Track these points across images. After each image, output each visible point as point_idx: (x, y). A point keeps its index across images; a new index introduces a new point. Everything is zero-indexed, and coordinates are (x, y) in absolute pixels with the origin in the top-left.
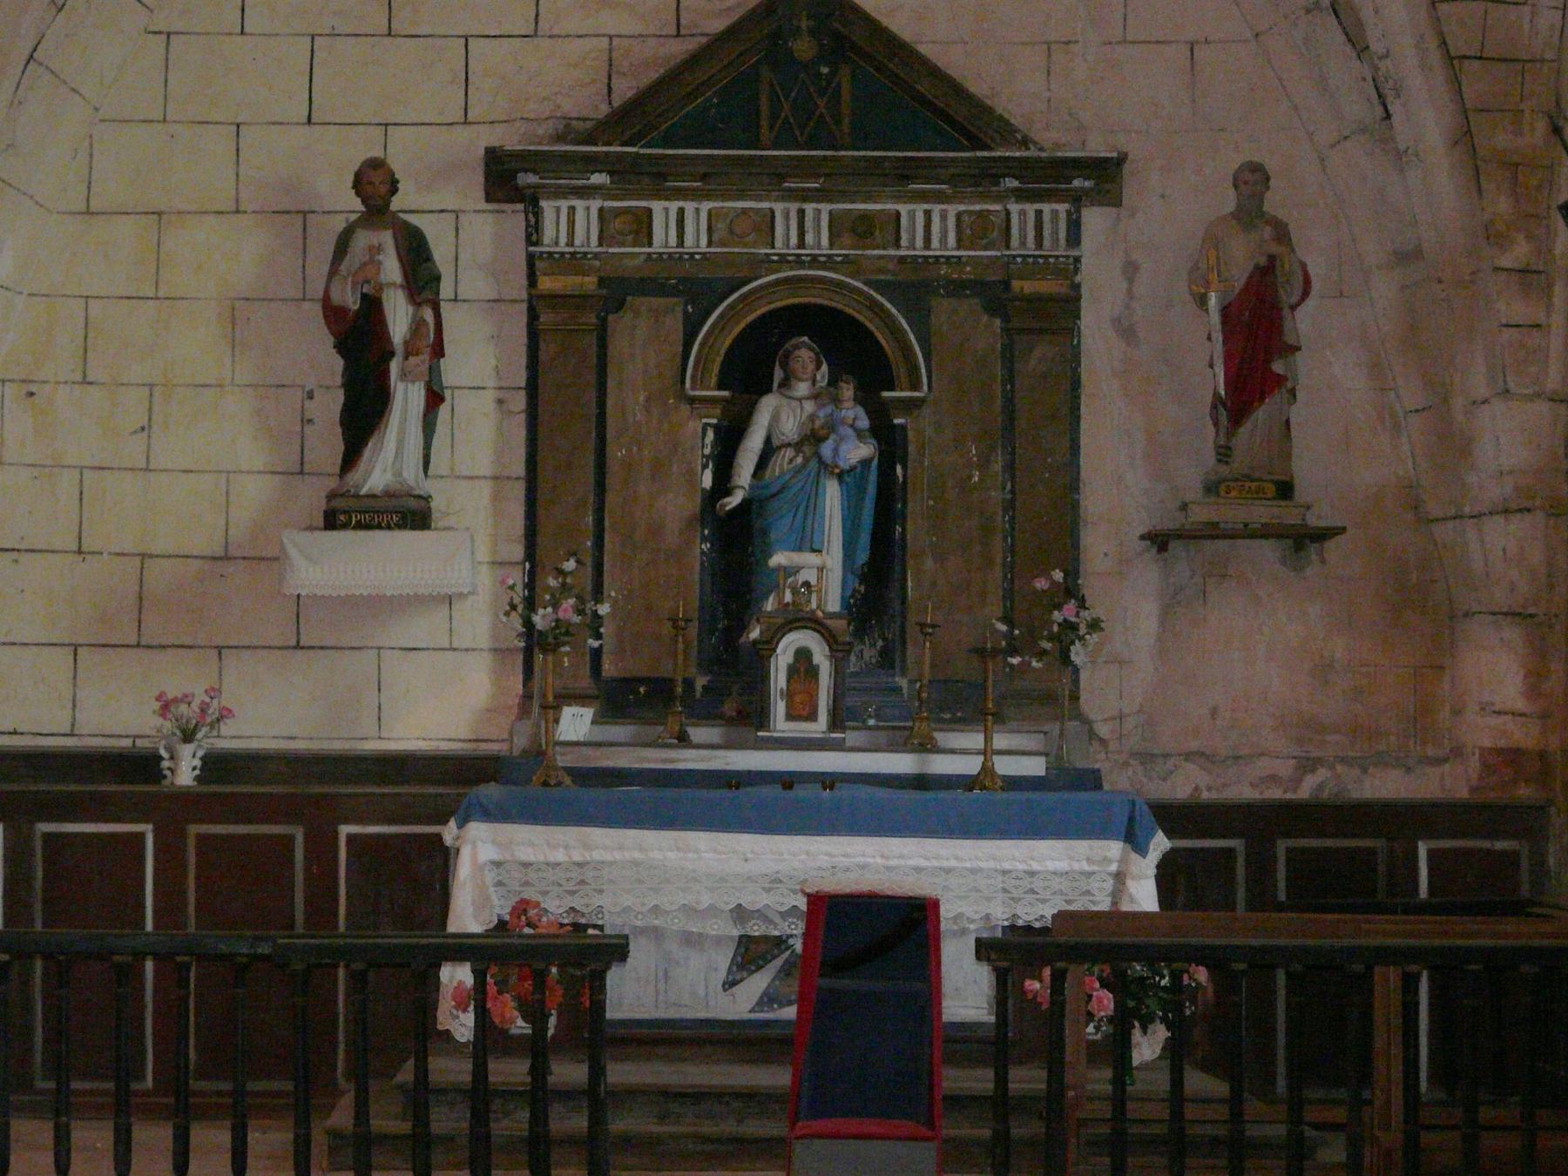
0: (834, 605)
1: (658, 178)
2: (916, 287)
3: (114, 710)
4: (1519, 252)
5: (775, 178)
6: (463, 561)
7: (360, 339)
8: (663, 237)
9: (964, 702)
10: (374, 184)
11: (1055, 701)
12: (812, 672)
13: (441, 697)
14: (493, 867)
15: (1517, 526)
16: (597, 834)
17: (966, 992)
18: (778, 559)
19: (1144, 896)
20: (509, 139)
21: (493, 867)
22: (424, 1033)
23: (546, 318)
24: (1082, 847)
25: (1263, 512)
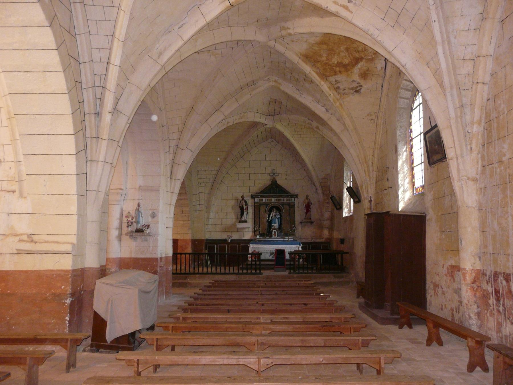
1: (263, 196)
2: (283, 204)
3: (224, 236)
4: (327, 201)
5: (272, 196)
6: (249, 225)
8: (264, 201)
9: (287, 235)
10: (243, 197)
11: (293, 235)
13: (248, 235)
14: (252, 248)
15: (328, 221)
17: (287, 257)
19: (300, 249)
21: (252, 248)
22: (247, 260)
25: (309, 220)
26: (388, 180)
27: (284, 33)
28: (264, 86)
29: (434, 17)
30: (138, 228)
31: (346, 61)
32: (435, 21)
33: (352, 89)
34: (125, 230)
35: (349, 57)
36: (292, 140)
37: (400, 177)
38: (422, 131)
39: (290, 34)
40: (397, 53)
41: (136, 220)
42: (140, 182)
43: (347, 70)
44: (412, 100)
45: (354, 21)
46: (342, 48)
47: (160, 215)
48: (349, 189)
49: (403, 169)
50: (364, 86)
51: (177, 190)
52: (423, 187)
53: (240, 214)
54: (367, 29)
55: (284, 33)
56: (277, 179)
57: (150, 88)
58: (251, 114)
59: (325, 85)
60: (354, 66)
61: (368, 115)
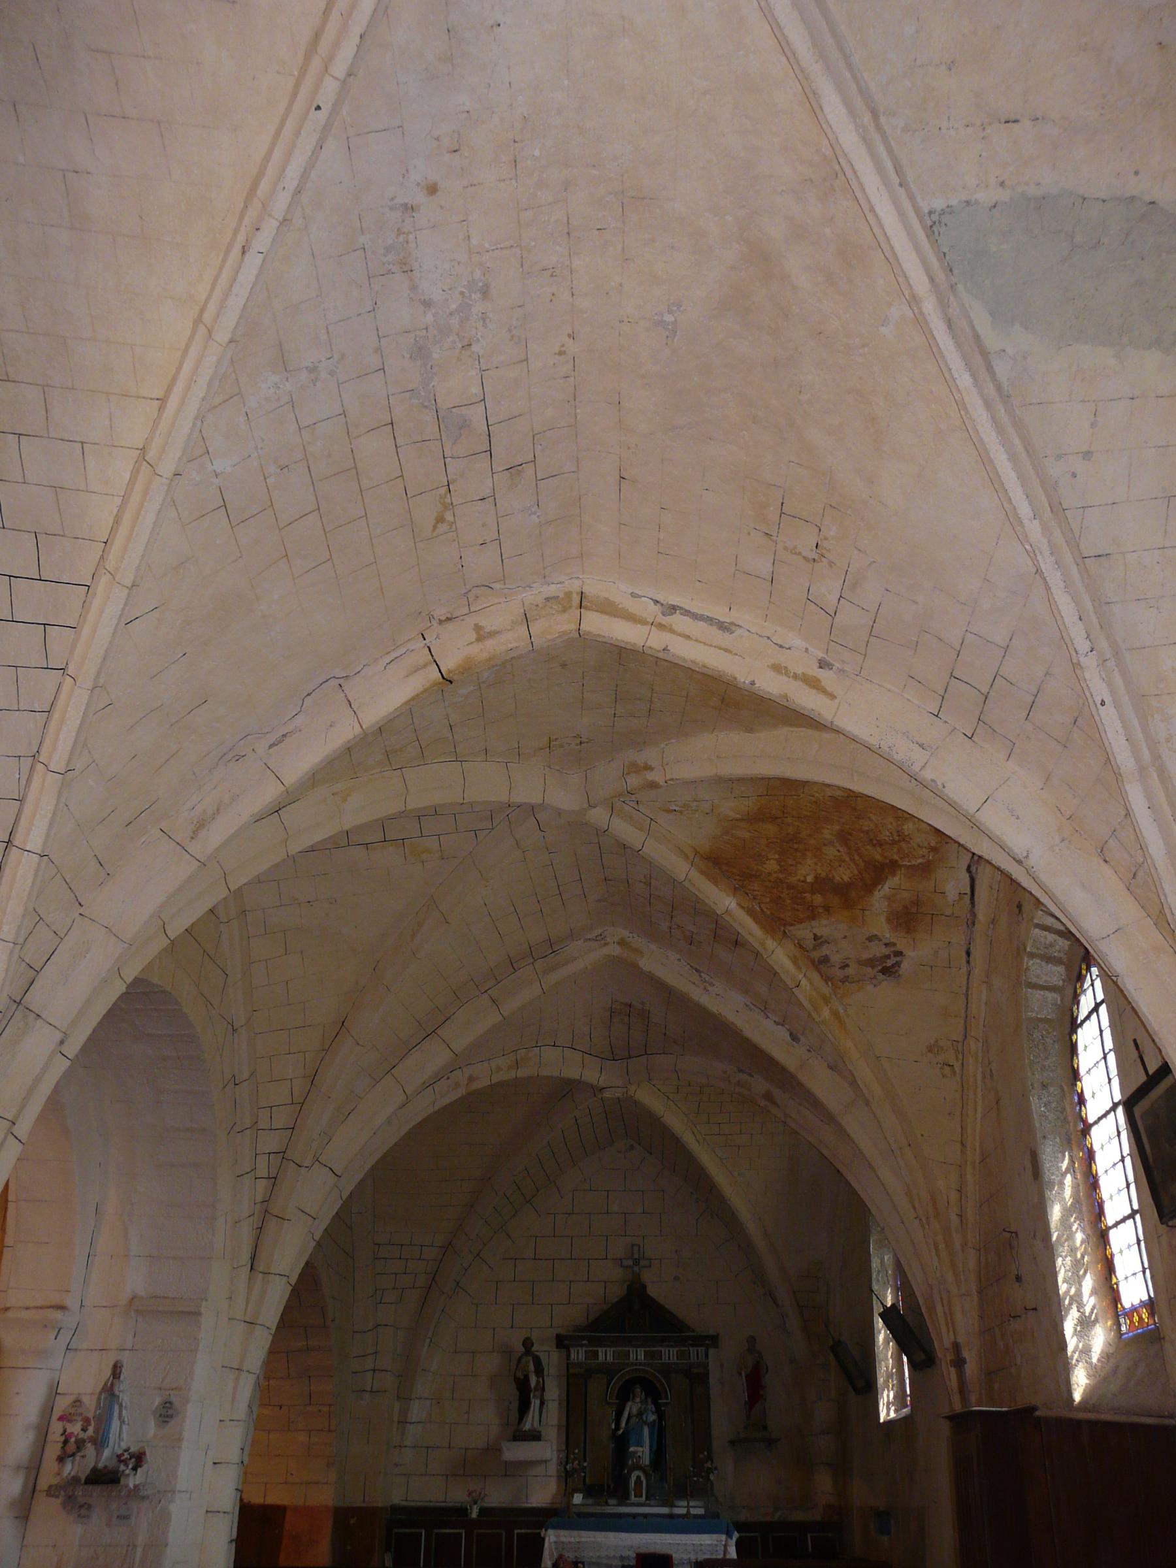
0: (647, 1462)
3: (457, 1495)
7: (523, 1387)
8: (601, 1358)
9: (682, 1491)
10: (527, 1343)
12: (641, 1482)
13: (542, 1492)
16: (583, 1533)
18: (632, 1449)
19: (732, 1553)
20: (560, 1331)
23: (571, 1371)
24: (715, 1536)
26: (1018, 1279)
27: (634, 781)
28: (584, 957)
29: (1099, 689)
30: (100, 1465)
31: (844, 875)
32: (1103, 703)
33: (870, 963)
34: (50, 1474)
35: (853, 860)
36: (689, 1139)
37: (1063, 1266)
38: (1118, 1097)
39: (653, 785)
40: (992, 819)
41: (96, 1431)
42: (136, 1281)
43: (848, 904)
44: (1069, 992)
45: (843, 723)
46: (827, 834)
47: (191, 1412)
48: (889, 1316)
49: (1071, 1237)
50: (909, 953)
51: (271, 1314)
52: (1150, 1305)
53: (515, 1405)
54: (885, 747)
55: (634, 781)
56: (647, 1277)
57: (165, 942)
58: (550, 1054)
59: (779, 951)
60: (869, 889)
61: (930, 1049)
